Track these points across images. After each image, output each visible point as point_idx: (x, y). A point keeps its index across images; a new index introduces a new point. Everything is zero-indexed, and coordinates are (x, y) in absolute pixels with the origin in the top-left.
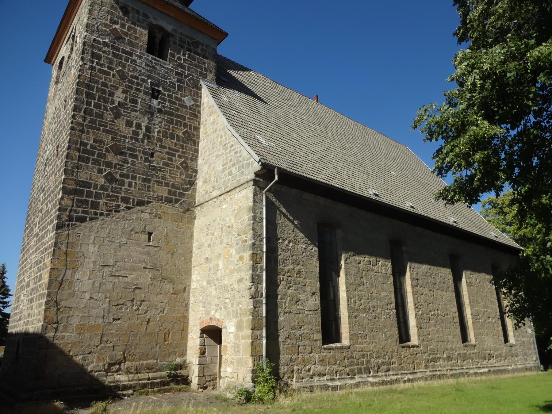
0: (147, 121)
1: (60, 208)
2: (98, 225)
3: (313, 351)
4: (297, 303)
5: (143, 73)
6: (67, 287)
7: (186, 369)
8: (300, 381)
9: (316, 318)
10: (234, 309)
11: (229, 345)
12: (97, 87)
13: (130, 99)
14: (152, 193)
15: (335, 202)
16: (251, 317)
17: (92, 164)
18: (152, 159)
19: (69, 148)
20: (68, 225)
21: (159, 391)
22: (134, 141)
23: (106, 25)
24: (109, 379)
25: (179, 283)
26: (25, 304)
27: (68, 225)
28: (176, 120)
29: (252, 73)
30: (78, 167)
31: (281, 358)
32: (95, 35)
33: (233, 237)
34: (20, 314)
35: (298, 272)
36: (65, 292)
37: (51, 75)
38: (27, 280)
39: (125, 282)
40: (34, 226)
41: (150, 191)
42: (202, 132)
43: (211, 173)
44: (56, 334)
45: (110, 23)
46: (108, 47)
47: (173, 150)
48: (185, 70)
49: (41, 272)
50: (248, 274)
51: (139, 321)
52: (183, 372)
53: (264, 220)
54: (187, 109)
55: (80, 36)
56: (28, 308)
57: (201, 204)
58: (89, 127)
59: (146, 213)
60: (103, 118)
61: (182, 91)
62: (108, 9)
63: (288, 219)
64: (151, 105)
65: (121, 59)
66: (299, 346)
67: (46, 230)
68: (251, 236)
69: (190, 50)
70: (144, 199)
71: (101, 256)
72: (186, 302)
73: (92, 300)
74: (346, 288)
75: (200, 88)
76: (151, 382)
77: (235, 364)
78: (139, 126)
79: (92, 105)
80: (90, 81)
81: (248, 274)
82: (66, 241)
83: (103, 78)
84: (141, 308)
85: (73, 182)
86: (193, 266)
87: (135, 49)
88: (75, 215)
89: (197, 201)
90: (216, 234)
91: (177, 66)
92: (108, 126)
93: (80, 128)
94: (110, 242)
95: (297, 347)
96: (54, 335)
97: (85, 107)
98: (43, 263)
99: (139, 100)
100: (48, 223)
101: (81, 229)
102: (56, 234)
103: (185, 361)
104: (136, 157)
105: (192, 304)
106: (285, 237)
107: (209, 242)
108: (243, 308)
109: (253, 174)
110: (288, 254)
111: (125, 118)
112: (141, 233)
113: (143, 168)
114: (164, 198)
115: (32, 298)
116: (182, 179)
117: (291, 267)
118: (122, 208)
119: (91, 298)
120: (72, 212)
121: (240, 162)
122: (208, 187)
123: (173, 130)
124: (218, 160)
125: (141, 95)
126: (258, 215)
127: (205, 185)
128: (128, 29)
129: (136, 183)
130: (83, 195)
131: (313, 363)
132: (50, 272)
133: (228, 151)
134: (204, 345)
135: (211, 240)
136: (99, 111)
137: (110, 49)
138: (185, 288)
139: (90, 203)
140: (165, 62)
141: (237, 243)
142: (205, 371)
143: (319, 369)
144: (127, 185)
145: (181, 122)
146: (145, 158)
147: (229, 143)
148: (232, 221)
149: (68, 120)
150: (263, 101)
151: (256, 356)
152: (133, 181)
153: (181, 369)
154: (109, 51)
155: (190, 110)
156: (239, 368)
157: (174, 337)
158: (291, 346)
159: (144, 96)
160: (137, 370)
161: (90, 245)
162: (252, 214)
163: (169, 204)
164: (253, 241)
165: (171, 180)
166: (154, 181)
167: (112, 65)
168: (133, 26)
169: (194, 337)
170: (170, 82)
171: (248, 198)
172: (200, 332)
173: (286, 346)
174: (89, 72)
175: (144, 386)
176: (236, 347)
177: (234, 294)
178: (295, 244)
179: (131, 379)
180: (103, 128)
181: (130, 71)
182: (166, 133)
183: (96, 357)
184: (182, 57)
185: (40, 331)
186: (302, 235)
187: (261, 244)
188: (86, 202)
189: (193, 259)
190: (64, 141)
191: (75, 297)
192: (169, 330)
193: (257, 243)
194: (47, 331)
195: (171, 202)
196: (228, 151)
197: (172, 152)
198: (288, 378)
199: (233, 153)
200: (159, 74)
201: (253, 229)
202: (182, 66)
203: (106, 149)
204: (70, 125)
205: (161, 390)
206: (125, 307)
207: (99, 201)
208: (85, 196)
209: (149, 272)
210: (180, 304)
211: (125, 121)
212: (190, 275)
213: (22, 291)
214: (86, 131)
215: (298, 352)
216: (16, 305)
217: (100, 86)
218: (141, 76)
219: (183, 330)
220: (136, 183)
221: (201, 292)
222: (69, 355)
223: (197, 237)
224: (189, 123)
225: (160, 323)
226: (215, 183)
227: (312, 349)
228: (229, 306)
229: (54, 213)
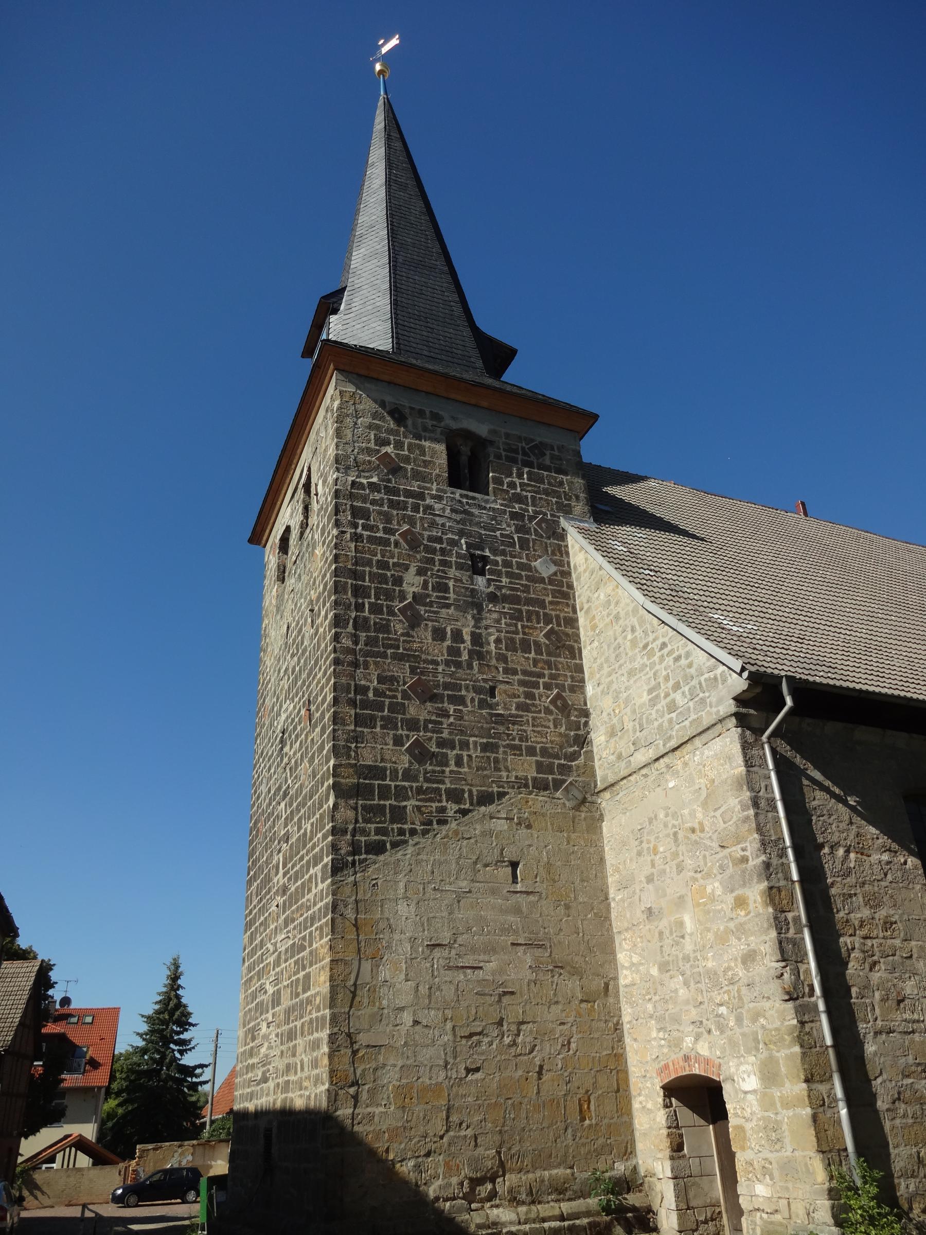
0: (472, 623)
1: (334, 828)
2: (408, 856)
4: (902, 1005)
5: (450, 527)
6: (366, 1001)
7: (640, 1191)
10: (746, 1030)
11: (748, 1126)
12: (370, 572)
13: (433, 586)
14: (504, 774)
16: (797, 1049)
17: (382, 727)
18: (494, 701)
19: (336, 701)
20: (354, 863)
23: (369, 451)
24: (477, 1218)
25: (593, 974)
26: (273, 1044)
27: (354, 863)
28: (528, 611)
29: (652, 483)
31: (893, 1156)
32: (353, 474)
33: (707, 853)
34: (264, 1066)
35: (885, 923)
36: (363, 1012)
37: (263, 566)
38: (270, 990)
39: (478, 981)
40: (273, 872)
41: (499, 770)
42: (585, 626)
43: (623, 712)
44: (357, 1111)
45: (376, 445)
46: (378, 492)
47: (531, 674)
48: (527, 505)
49: (307, 970)
50: (767, 938)
51: (520, 1073)
52: (632, 1199)
53: (780, 805)
54: (545, 583)
55: (324, 482)
56: (282, 1052)
57: (612, 785)
58: (367, 654)
59: (498, 818)
60: (389, 632)
61: (528, 550)
62: (367, 420)
63: (833, 795)
64: (473, 589)
65: (405, 508)
67: (307, 877)
68: (757, 845)
70: (490, 790)
72: (615, 1020)
73: (417, 1028)
75: (562, 536)
77: (776, 1173)
78: (457, 636)
79: (367, 609)
80: (356, 564)
81: (767, 938)
82: (354, 898)
83: (379, 552)
84: (520, 1040)
85: (351, 770)
86: (615, 930)
88: (363, 839)
89: (599, 779)
90: (661, 849)
91: (510, 500)
92: (401, 644)
93: (350, 658)
94: (437, 892)
96: (353, 1113)
97: (353, 615)
98: (308, 950)
99: (451, 584)
100: (308, 862)
101: (378, 869)
102: (333, 883)
103: (635, 1169)
104: (461, 701)
105: (629, 1022)
107: (647, 870)
108: (770, 1027)
109: (732, 702)
110: (851, 880)
111: (430, 624)
112: (496, 864)
113: (479, 722)
115: (291, 1029)
116: (560, 733)
117: (866, 913)
118: (451, 814)
119: (416, 1023)
120: (358, 834)
121: (693, 677)
122: (622, 743)
123: (524, 633)
124: (635, 682)
125: (453, 572)
126: (761, 794)
127: (613, 740)
128: (409, 450)
129: (469, 756)
130: (373, 795)
132: (331, 969)
133: (656, 658)
134: (677, 1127)
135: (653, 866)
136: (381, 619)
137: (382, 495)
138: (607, 986)
139: (388, 811)
140: (487, 497)
141: (721, 867)
142: (691, 1194)
144: (452, 762)
145: (537, 613)
147: (654, 640)
148: (699, 815)
149: (323, 645)
150: (694, 537)
151: (830, 1151)
152: (465, 753)
154: (382, 499)
155: (550, 584)
156: (790, 1185)
157: (601, 1107)
158: (910, 1121)
159: (458, 574)
160: (532, 1195)
161: (400, 902)
162: (748, 794)
164: (763, 858)
166: (504, 747)
167: (391, 523)
169: (649, 1106)
170: (502, 535)
171: (729, 758)
172: (661, 1093)
173: (898, 1122)
174: (353, 545)
176: (772, 1129)
177: (739, 991)
178: (862, 854)
180: (392, 651)
181: (424, 529)
182: (512, 640)
183: (442, 1164)
184: (517, 481)
185: (324, 1104)
186: (873, 830)
187: (783, 864)
189: (613, 915)
190: (322, 689)
191: (384, 1022)
192: (587, 1091)
193: (775, 861)
194: (339, 1103)
195: (546, 788)
196: (656, 658)
197: (531, 679)
199: (669, 660)
201: (759, 829)
202: (519, 499)
204: (333, 655)
206: (486, 1040)
207: (404, 803)
208: (376, 797)
210: (603, 1025)
211: (430, 629)
212: (613, 953)
213: (261, 1014)
214: (361, 662)
216: (248, 1047)
217: (375, 570)
218: (446, 534)
219: (618, 1091)
220: (469, 756)
221: (649, 993)
222: (387, 1160)
223: (613, 862)
224: (553, 613)
225: (566, 1074)
226: (638, 734)
228: (732, 1024)
229: (322, 841)
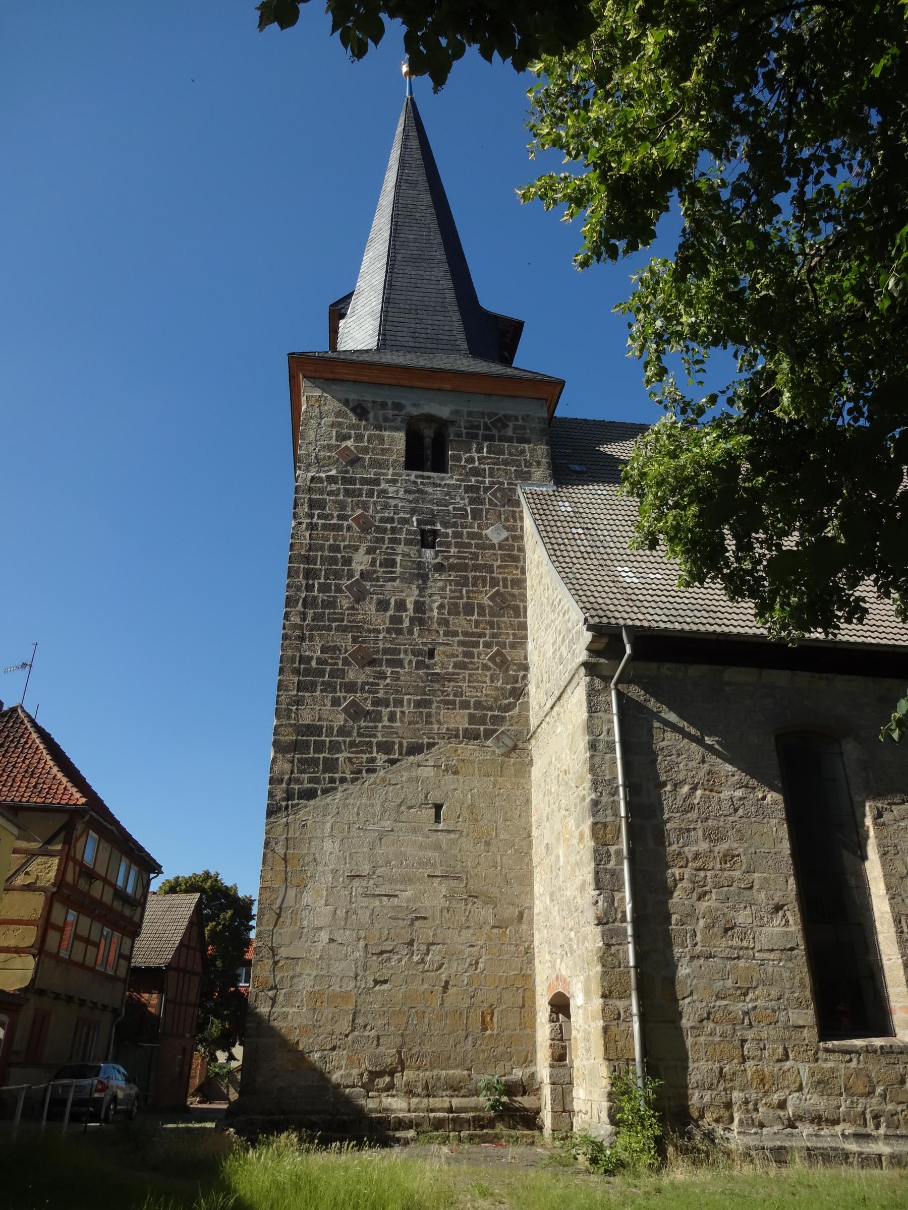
0: (417, 592)
2: (337, 801)
3: (791, 1056)
4: (730, 933)
6: (289, 921)
8: (753, 1131)
9: (792, 970)
13: (381, 562)
14: (436, 726)
15: (825, 675)
16: (599, 968)
17: (322, 691)
20: (287, 807)
21: (471, 1138)
22: (394, 636)
23: (329, 447)
25: (509, 903)
27: (287, 807)
30: (298, 702)
31: (690, 1069)
35: (725, 856)
36: (285, 930)
39: (393, 907)
41: (431, 723)
44: (274, 1010)
51: (426, 986)
52: (525, 1101)
54: (495, 549)
58: (313, 628)
60: (335, 607)
66: (743, 1041)
69: (490, 438)
70: (420, 741)
71: (345, 859)
72: (527, 944)
73: (332, 945)
74: (888, 888)
76: (453, 1117)
78: (401, 606)
80: (310, 550)
84: (428, 958)
87: (383, 471)
88: (297, 787)
91: (467, 475)
92: (346, 618)
95: (737, 1043)
97: (303, 595)
99: (398, 559)
101: (309, 812)
104: (400, 663)
106: (681, 777)
110: (693, 815)
111: (375, 597)
112: (420, 807)
113: (415, 681)
114: (461, 733)
116: (497, 687)
117: (704, 846)
118: (380, 763)
119: (332, 940)
125: (401, 549)
126: (601, 737)
129: (403, 712)
130: (309, 749)
131: (794, 1087)
138: (521, 915)
139: (321, 763)
143: (813, 1105)
144: (386, 718)
145: (484, 578)
146: (418, 663)
151: (617, 1059)
152: (398, 710)
153: (524, 1094)
158: (717, 1039)
160: (428, 1090)
161: (325, 840)
163: (472, 742)
164: (593, 796)
165: (474, 694)
167: (345, 510)
168: (378, 432)
170: (455, 509)
172: (549, 1008)
173: (702, 1039)
174: (307, 534)
175: (438, 1124)
178: (711, 791)
179: (413, 1107)
181: (377, 512)
182: (456, 605)
183: (346, 1057)
184: (476, 455)
186: (729, 767)
187: (614, 801)
188: (315, 761)
191: (303, 939)
192: (492, 1005)
193: (605, 799)
195: (477, 737)
198: (717, 1121)
200: (431, 501)
201: (593, 770)
202: (476, 472)
203: (345, 659)
205: (476, 1136)
206: (396, 957)
207: (337, 756)
208: (312, 752)
209: (441, 883)
212: (531, 885)
215: (743, 1056)
219: (523, 1006)
220: (403, 712)
224: (501, 576)
225: (471, 989)
227: (785, 1049)
